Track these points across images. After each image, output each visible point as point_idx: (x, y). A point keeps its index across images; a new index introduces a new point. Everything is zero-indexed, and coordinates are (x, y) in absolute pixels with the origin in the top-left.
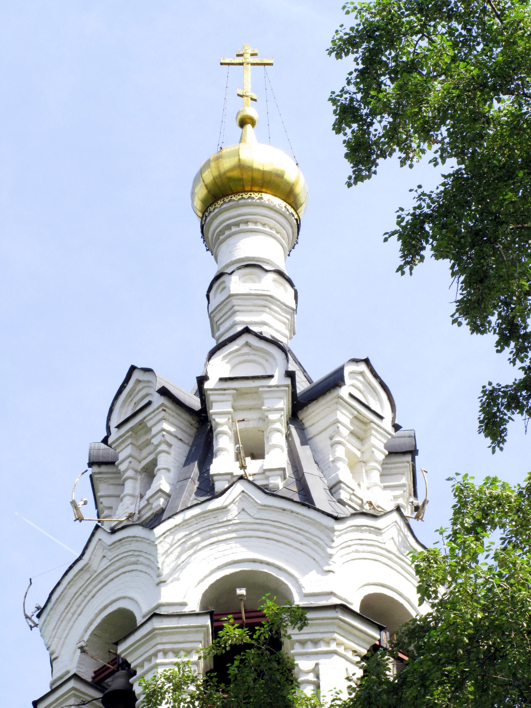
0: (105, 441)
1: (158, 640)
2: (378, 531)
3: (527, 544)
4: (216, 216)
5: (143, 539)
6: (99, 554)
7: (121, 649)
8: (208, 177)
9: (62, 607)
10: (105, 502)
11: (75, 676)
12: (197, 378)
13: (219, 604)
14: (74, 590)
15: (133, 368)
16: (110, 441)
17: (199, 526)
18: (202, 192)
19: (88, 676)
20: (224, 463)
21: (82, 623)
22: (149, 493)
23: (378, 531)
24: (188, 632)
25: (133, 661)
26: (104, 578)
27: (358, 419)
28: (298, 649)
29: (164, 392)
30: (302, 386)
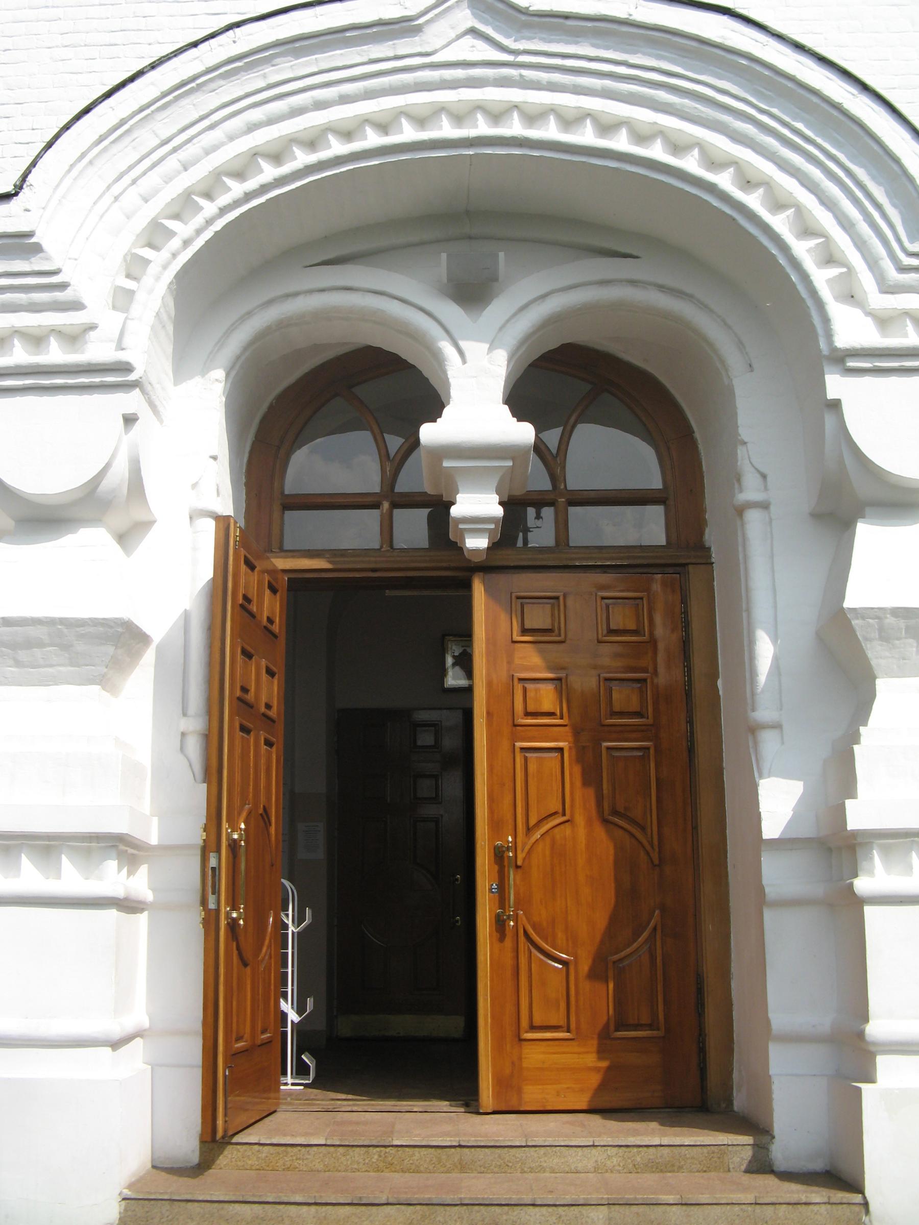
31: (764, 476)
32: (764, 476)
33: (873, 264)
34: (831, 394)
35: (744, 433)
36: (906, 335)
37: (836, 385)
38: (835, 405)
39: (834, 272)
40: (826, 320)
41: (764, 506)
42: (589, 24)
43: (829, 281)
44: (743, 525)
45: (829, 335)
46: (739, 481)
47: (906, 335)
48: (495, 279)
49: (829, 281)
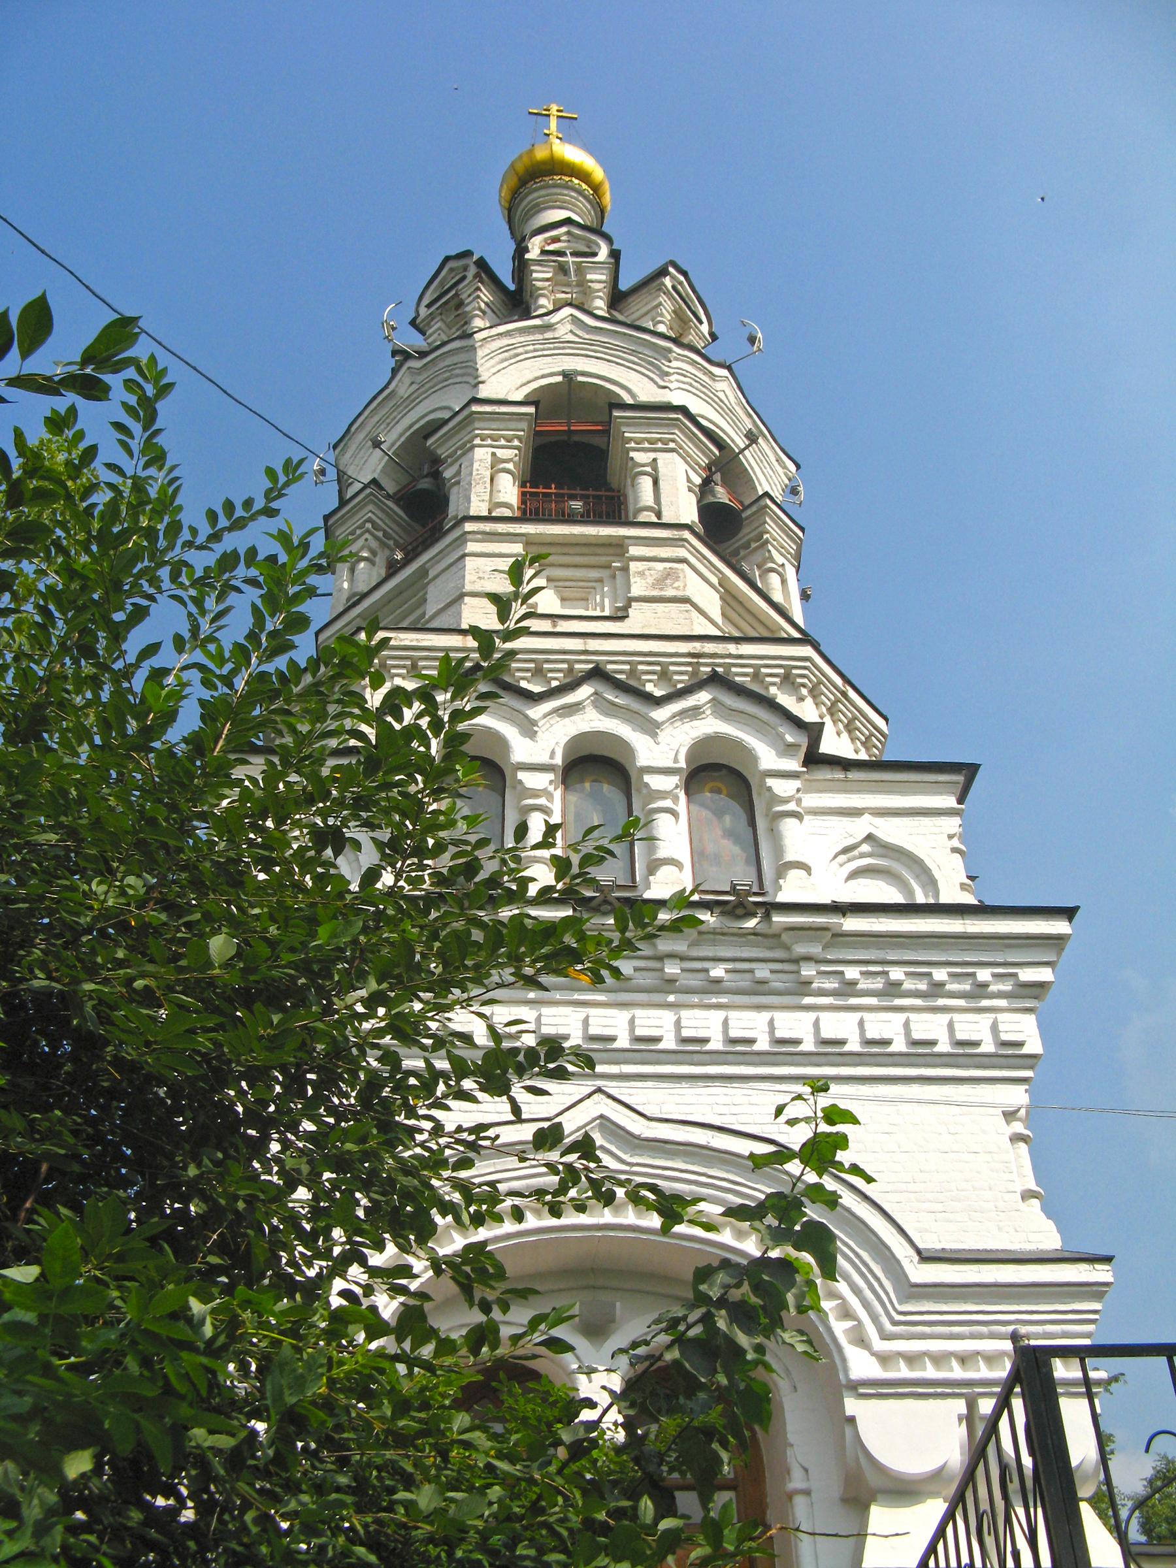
1: (477, 425)
3: (204, 1257)
4: (526, 196)
6: (407, 381)
7: (429, 442)
8: (520, 168)
14: (376, 418)
16: (418, 321)
17: (522, 339)
24: (509, 420)
25: (443, 452)
27: (677, 313)
31: (806, 1470)
32: (806, 1470)
33: (875, 1319)
34: (849, 1412)
35: (791, 1437)
36: (899, 1370)
37: (852, 1406)
38: (852, 1420)
39: (849, 1324)
40: (844, 1360)
41: (807, 1493)
42: (682, 1148)
43: (846, 1331)
44: (792, 1507)
45: (846, 1370)
46: (789, 1474)
47: (899, 1370)
48: (613, 1321)
49: (846, 1331)
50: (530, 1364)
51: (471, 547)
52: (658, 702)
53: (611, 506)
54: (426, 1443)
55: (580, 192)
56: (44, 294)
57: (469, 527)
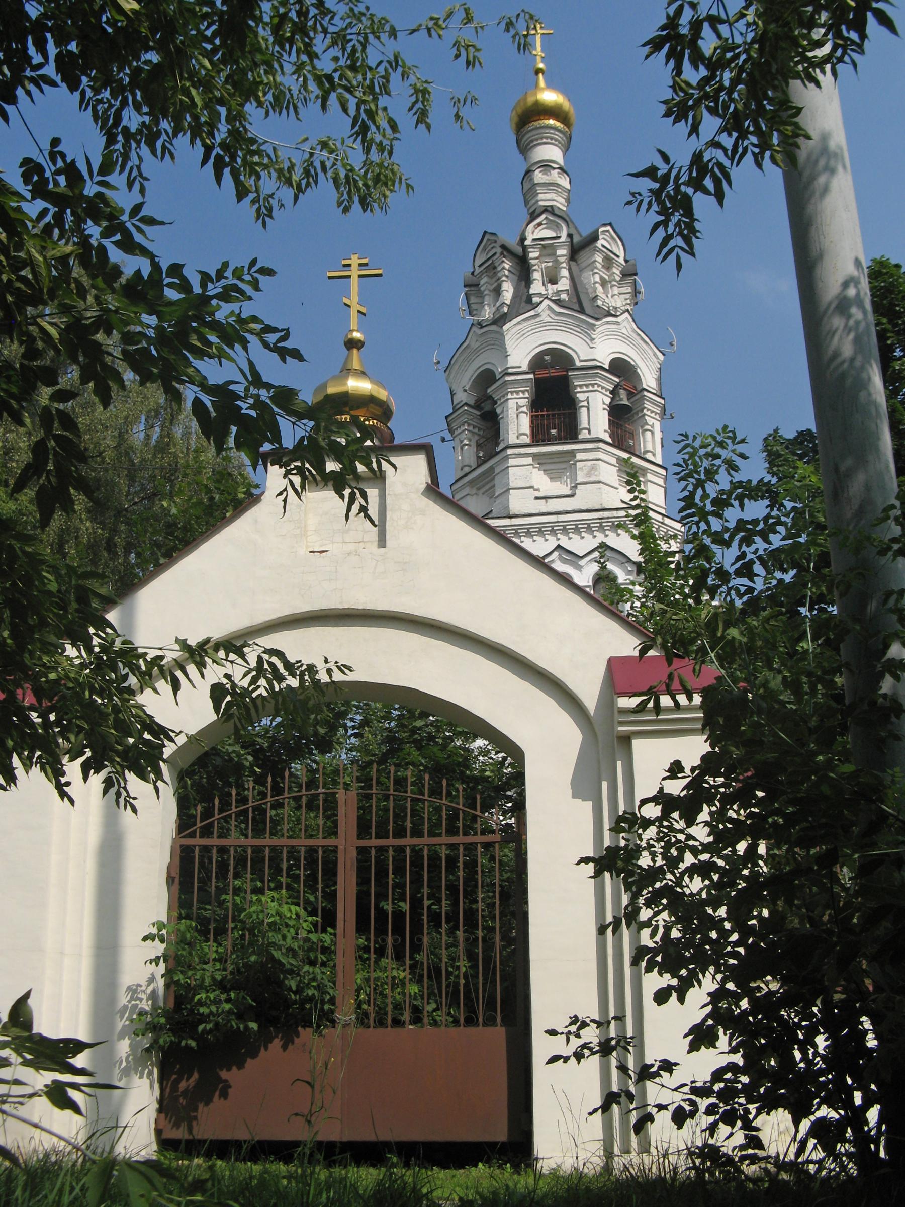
0: (473, 273)
2: (618, 323)
5: (497, 332)
6: (474, 339)
8: (520, 110)
9: (456, 367)
10: (474, 307)
11: (466, 404)
12: (575, 796)
13: (537, 363)
15: (485, 233)
18: (516, 119)
19: (472, 403)
20: (537, 287)
21: (465, 379)
22: (498, 304)
23: (618, 323)
26: (477, 352)
28: (579, 389)
29: (503, 247)
30: (576, 239)
50: (114, 386)
51: (512, 462)
52: (582, 557)
53: (571, 432)
54: (292, 930)
55: (555, 129)
56: (689, 1052)
57: (509, 451)
